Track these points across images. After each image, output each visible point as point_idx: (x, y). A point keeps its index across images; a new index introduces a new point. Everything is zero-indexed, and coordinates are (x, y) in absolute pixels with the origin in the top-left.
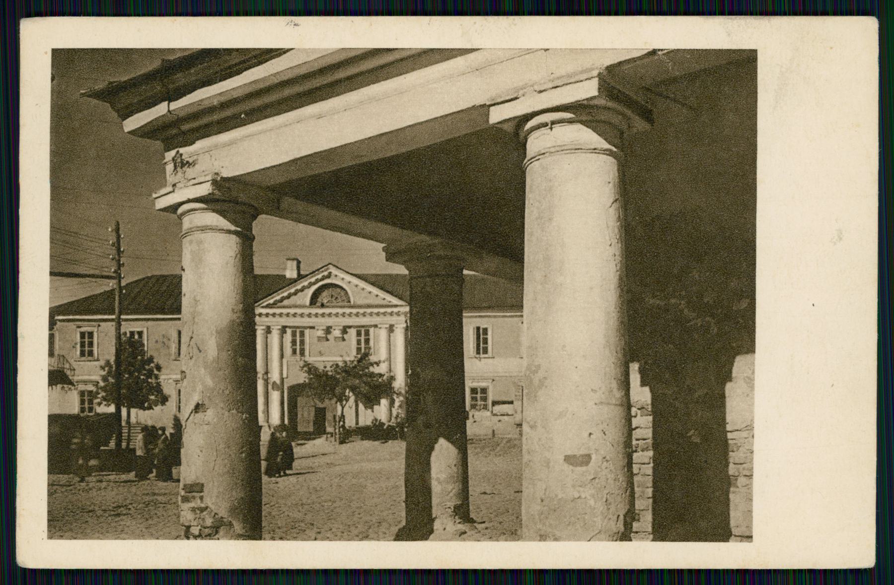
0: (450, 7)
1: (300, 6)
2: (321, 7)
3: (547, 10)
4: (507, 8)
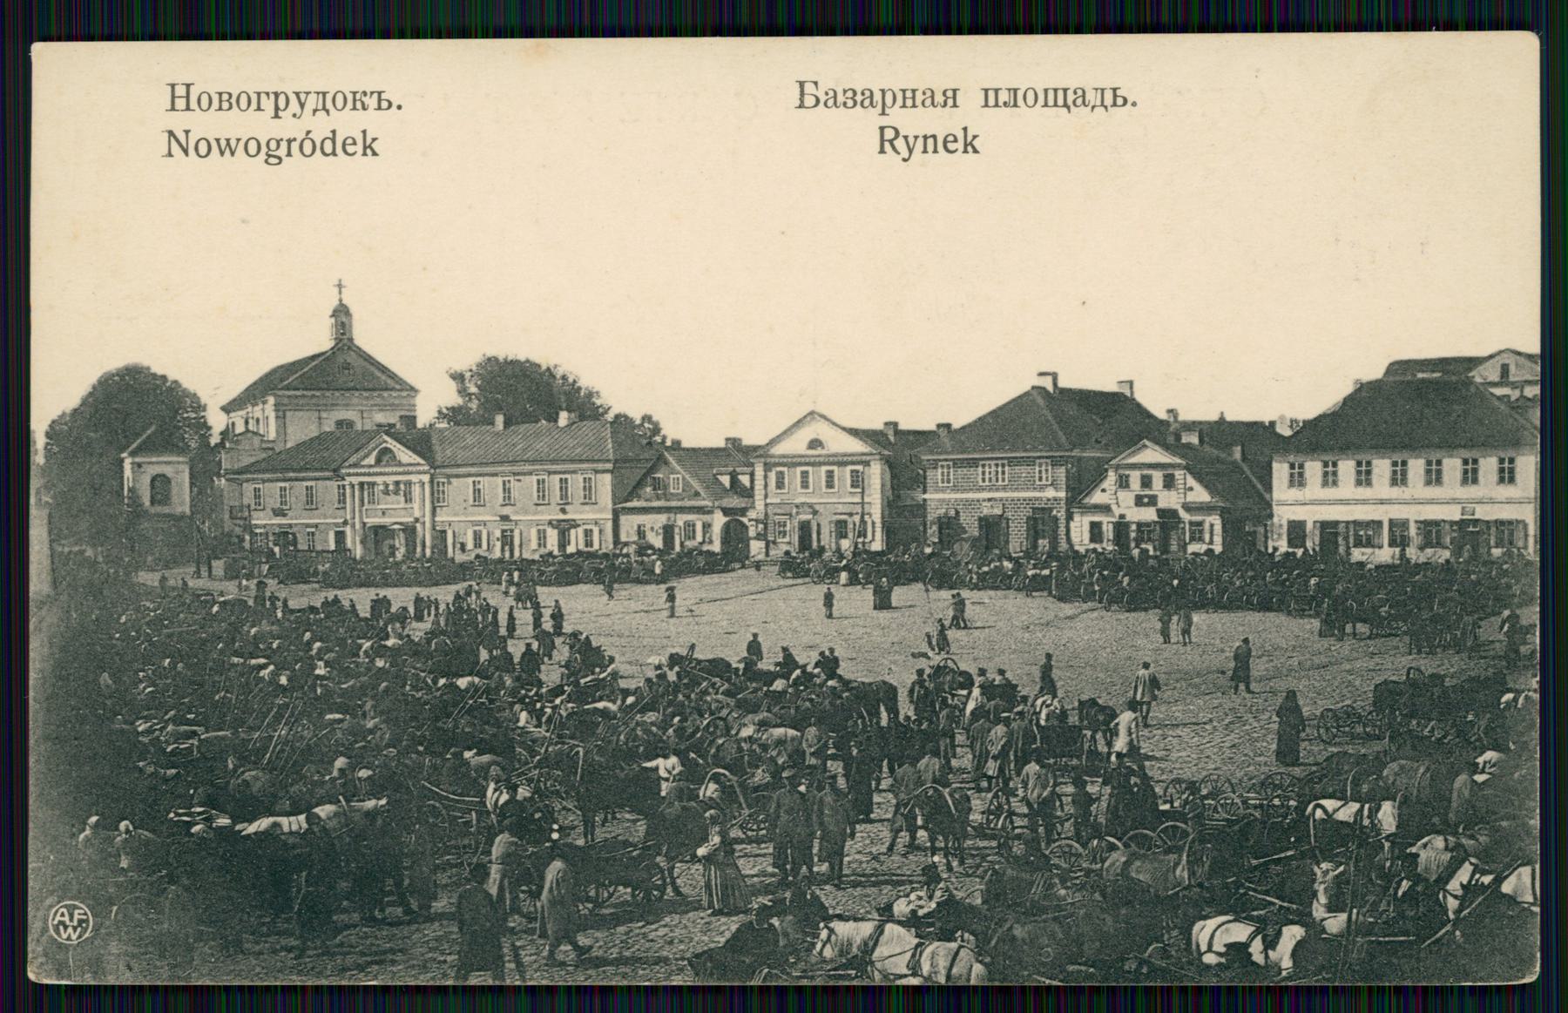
0: (781, 19)
1: (514, 19)
2: (551, 20)
3: (954, 25)
4: (883, 20)
